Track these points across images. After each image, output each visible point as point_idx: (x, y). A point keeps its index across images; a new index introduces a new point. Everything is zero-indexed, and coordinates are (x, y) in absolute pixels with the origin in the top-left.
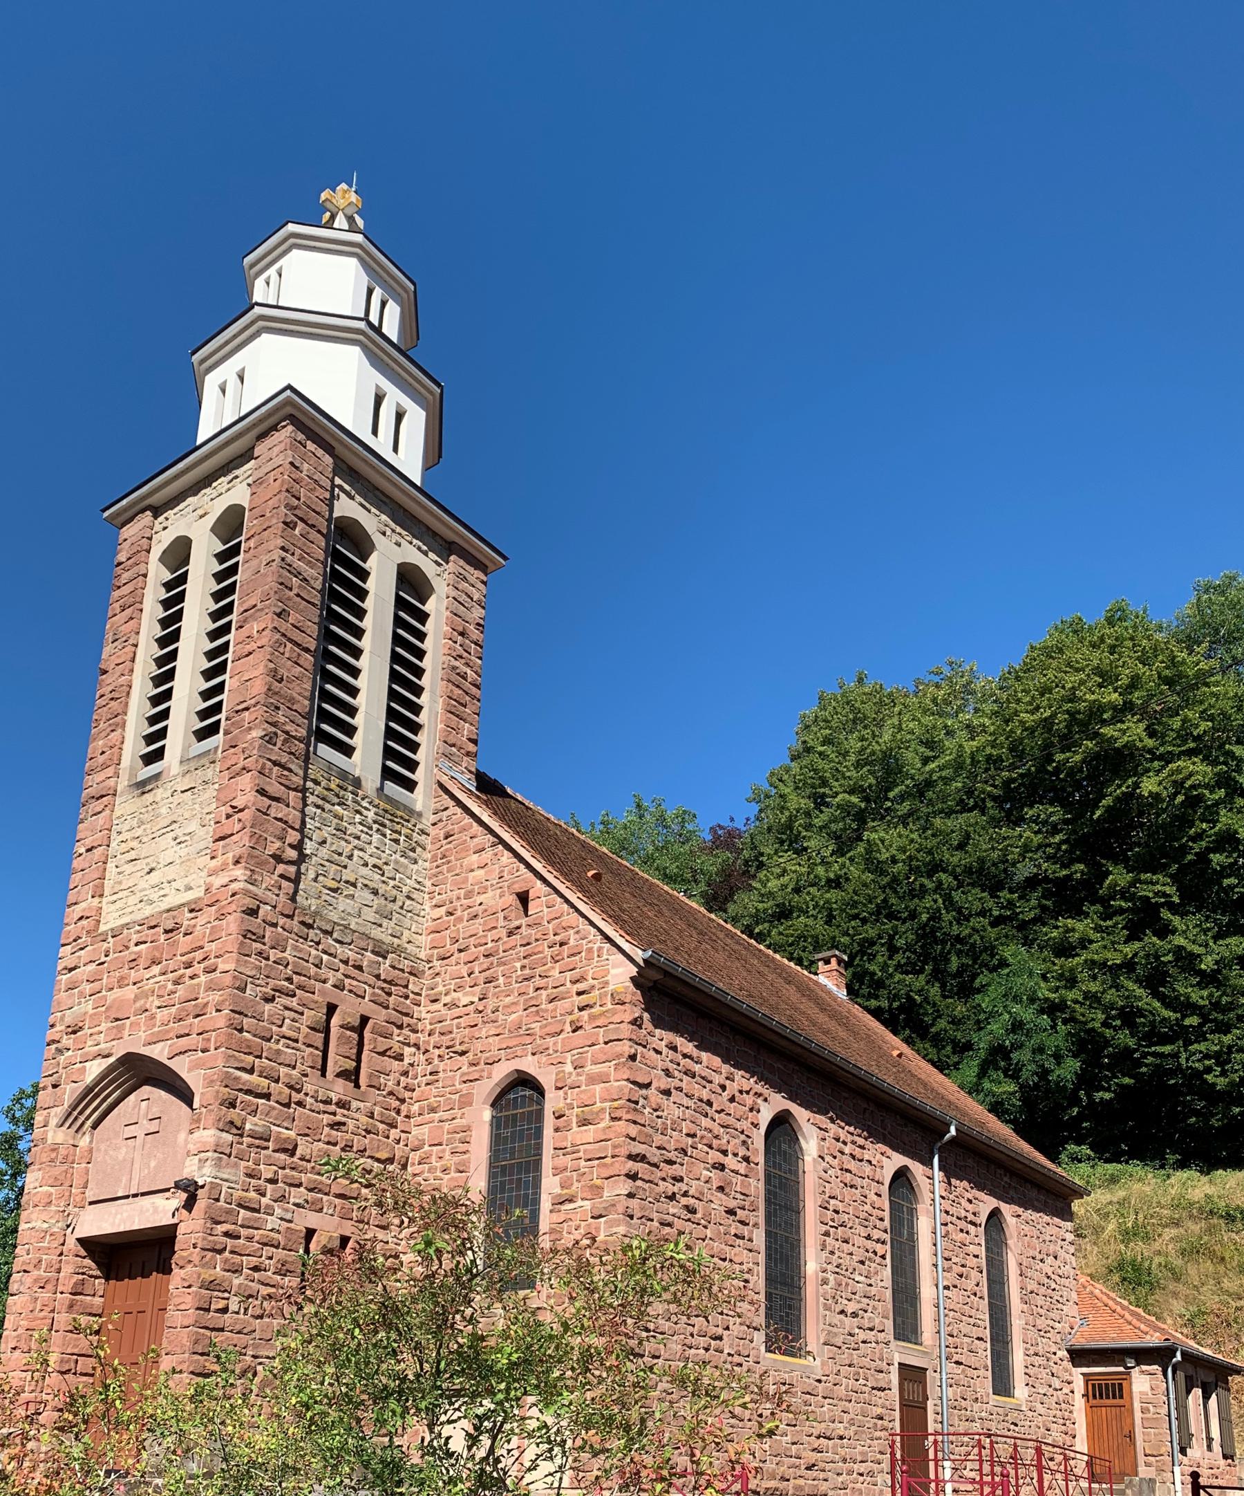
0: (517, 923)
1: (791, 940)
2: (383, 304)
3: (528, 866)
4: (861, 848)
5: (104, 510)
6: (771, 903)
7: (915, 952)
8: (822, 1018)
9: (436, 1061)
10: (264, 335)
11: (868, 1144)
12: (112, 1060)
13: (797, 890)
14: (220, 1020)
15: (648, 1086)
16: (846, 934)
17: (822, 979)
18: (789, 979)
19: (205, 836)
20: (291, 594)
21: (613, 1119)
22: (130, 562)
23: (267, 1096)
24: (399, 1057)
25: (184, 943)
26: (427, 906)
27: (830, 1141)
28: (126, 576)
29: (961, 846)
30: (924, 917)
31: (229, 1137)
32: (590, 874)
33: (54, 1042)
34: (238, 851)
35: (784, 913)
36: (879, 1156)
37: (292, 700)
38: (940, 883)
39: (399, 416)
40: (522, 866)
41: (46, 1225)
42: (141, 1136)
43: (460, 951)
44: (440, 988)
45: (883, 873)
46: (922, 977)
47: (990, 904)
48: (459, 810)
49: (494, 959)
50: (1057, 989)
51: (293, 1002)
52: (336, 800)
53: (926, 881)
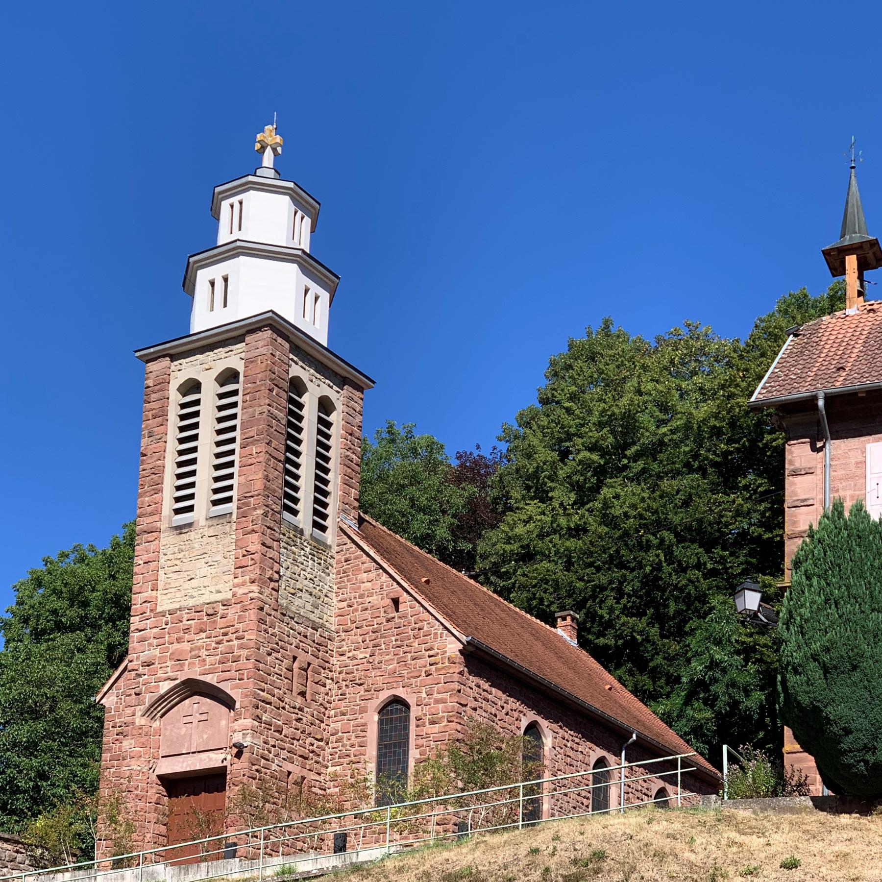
0: (392, 615)
1: (534, 582)
2: (302, 218)
3: (398, 583)
4: (598, 505)
5: (136, 352)
6: (517, 545)
7: (640, 597)
8: (558, 665)
9: (344, 688)
10: (241, 257)
11: (581, 742)
12: (177, 682)
13: (541, 536)
14: (250, 664)
15: (466, 705)
16: (581, 579)
17: (559, 631)
18: (536, 634)
19: (231, 563)
20: (273, 430)
21: (449, 721)
22: (156, 387)
23: (270, 704)
24: (324, 685)
25: (221, 623)
26: (335, 600)
27: (559, 740)
28: (154, 396)
29: (686, 503)
30: (648, 569)
31: (257, 724)
32: (424, 580)
33: (133, 670)
34: (253, 576)
35: (527, 556)
36: (587, 749)
37: (275, 491)
38: (662, 540)
39: (317, 298)
40: (395, 583)
41: (139, 768)
42: (195, 721)
43: (357, 628)
44: (345, 648)
45: (616, 527)
46: (644, 619)
47: (705, 558)
48: (354, 546)
49: (378, 634)
50: (751, 635)
51: (279, 656)
52: (292, 543)
53: (652, 538)
